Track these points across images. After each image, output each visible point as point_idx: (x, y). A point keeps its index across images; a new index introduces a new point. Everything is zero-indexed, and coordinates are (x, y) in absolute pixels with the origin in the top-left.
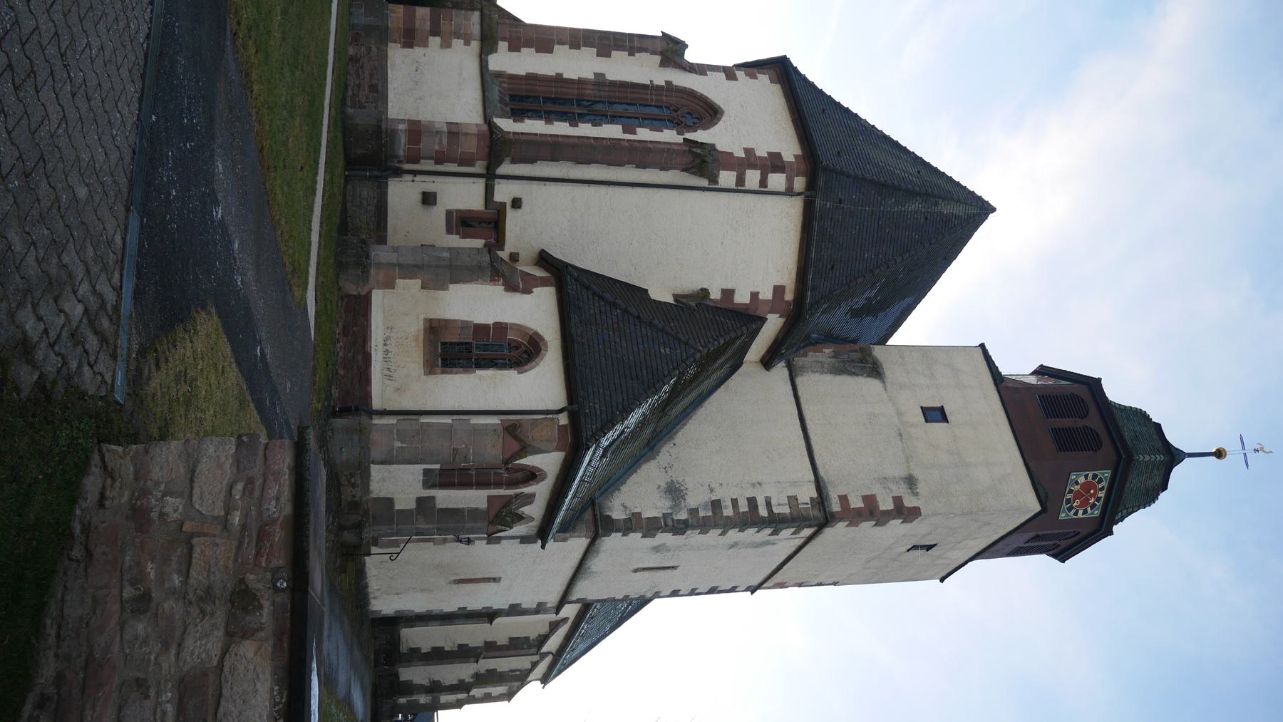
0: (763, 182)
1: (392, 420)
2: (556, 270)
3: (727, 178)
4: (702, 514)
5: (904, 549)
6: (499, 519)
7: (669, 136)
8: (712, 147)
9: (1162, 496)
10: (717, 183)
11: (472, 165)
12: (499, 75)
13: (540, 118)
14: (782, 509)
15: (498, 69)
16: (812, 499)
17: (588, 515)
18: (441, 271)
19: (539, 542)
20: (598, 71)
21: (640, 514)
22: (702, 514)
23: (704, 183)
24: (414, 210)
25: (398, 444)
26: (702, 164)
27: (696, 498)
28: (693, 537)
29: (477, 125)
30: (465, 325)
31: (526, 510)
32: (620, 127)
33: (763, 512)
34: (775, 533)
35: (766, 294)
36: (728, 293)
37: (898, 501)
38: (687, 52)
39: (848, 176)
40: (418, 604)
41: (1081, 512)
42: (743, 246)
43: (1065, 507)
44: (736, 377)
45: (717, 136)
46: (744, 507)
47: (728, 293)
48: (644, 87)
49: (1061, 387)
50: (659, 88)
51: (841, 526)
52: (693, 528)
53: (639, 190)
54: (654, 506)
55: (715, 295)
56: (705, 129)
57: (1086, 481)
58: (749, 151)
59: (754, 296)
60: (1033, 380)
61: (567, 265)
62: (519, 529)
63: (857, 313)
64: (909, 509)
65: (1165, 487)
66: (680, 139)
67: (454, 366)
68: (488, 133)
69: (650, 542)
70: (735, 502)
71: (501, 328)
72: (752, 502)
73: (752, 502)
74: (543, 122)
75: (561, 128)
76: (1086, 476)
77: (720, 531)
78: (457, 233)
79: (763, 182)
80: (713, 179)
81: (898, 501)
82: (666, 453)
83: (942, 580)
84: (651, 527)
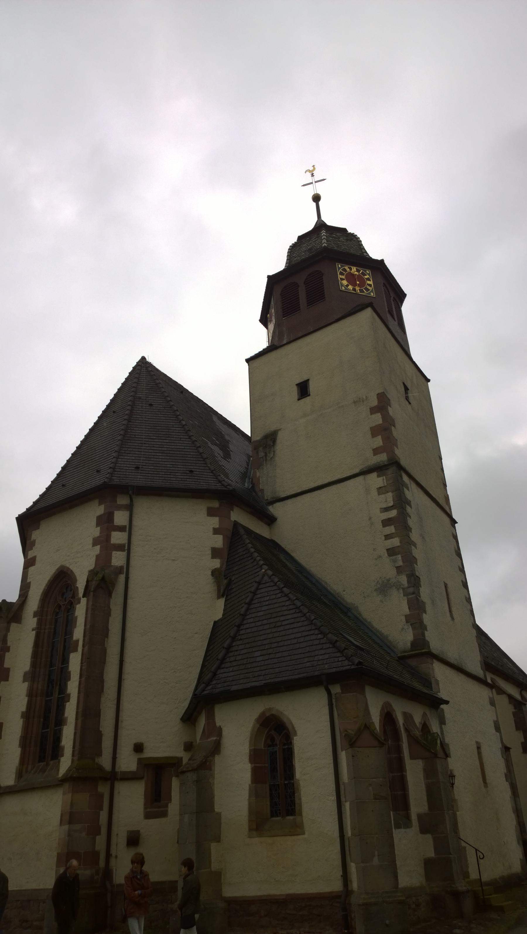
0: (121, 529)
1: (353, 868)
2: (203, 703)
3: (118, 559)
4: (400, 563)
5: (409, 407)
6: (432, 749)
7: (81, 611)
8: (93, 573)
9: (350, 231)
10: (122, 568)
11: (101, 796)
12: (20, 774)
13: (60, 731)
14: (389, 499)
15: (14, 776)
16: (378, 476)
17: (413, 662)
18: (204, 819)
19: (442, 706)
20: (21, 679)
21: (406, 616)
22: (400, 563)
23: (122, 578)
24: (145, 835)
25: (376, 861)
26: (105, 582)
27: (388, 569)
28: (421, 569)
29: (64, 794)
30: (254, 793)
31: (418, 720)
33: (393, 513)
34: (409, 503)
35: (215, 522)
36: (215, 553)
37: (373, 410)
38: (9, 600)
40: (509, 821)
41: (368, 282)
42: (175, 550)
44: (283, 545)
45: (82, 570)
46: (391, 529)
47: (215, 553)
48: (37, 636)
49: (276, 312)
50: (39, 623)
51: (398, 452)
53: (128, 634)
54: (400, 605)
55: (216, 563)
56: (76, 580)
57: (343, 278)
58: (95, 542)
59: (216, 531)
60: (271, 326)
61: (195, 695)
62: (435, 728)
63: (227, 455)
64: (379, 401)
65: (344, 230)
66: (84, 601)
67: (293, 803)
69: (429, 607)
70: (388, 537)
71: (255, 756)
72: (386, 523)
73: (386, 523)
75: (71, 710)
76: (342, 279)
77: (413, 547)
78: (166, 806)
79: (121, 529)
80: (119, 570)
81: (373, 410)
82: (351, 597)
83: (429, 380)
84: (417, 607)
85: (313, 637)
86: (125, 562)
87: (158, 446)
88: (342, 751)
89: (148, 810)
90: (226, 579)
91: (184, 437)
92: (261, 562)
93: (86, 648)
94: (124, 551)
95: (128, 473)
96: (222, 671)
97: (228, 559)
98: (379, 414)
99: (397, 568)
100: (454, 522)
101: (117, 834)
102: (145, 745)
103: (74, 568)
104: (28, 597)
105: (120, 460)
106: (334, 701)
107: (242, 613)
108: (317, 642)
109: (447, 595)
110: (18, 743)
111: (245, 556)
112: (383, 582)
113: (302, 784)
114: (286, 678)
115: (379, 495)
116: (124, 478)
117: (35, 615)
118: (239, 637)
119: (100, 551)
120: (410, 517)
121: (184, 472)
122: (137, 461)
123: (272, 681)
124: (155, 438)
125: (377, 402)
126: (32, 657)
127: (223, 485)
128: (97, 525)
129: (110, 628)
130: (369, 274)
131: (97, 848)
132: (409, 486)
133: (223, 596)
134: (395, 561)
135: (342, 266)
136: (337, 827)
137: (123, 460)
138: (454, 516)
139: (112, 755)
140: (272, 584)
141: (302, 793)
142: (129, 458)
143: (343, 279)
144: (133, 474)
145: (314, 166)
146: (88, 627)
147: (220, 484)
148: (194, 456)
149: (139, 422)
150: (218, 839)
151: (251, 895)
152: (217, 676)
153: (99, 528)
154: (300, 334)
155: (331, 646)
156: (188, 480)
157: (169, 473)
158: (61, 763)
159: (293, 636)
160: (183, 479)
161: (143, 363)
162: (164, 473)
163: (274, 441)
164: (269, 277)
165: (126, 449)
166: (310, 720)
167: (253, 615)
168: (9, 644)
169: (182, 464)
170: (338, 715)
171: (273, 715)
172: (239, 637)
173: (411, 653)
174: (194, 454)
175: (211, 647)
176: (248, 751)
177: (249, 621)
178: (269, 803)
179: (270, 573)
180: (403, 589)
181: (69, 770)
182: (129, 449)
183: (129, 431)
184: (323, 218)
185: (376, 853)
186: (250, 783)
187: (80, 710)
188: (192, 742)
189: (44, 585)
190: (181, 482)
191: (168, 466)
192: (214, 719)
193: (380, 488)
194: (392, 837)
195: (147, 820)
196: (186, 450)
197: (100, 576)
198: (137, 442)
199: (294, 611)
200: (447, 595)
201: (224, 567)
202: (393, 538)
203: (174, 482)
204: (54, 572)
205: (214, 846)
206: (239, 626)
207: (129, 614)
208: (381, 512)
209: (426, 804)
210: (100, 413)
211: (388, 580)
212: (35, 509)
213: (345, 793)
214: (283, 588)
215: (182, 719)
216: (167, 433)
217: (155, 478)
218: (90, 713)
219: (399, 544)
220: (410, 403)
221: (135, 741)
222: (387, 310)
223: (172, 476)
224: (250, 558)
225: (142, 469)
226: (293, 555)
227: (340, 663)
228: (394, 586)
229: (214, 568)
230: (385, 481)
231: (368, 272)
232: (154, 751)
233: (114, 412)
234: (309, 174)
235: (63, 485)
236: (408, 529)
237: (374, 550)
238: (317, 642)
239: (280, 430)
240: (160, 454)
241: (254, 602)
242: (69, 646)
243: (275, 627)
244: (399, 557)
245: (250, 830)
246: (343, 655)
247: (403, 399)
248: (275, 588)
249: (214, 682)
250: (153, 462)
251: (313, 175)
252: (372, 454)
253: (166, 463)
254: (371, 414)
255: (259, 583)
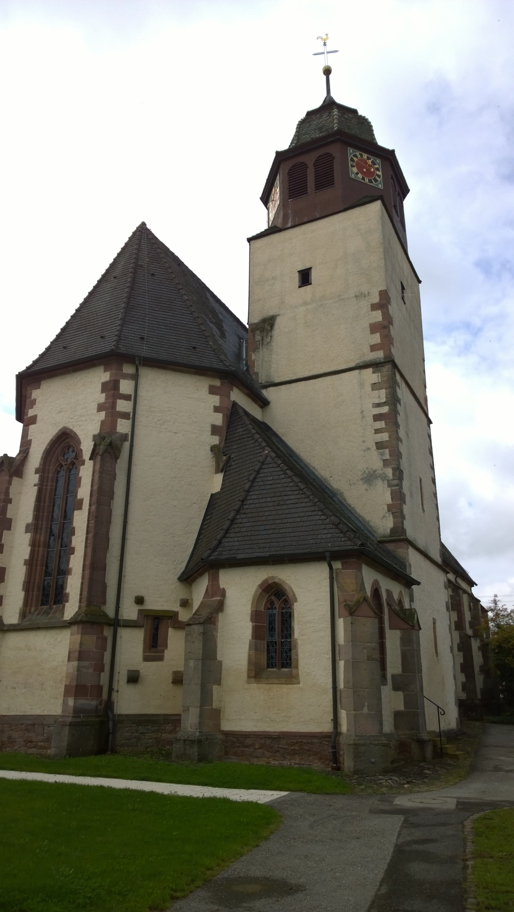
0: (127, 398)
1: (343, 714)
3: (123, 427)
4: (387, 457)
5: (404, 306)
7: (86, 473)
8: (98, 439)
9: (361, 112)
10: (126, 435)
11: (105, 639)
12: (23, 615)
14: (382, 395)
15: (17, 616)
16: (374, 372)
17: (391, 547)
19: (414, 587)
20: (24, 529)
22: (387, 457)
23: (127, 444)
25: (365, 710)
26: (111, 448)
27: (375, 461)
29: (72, 634)
30: (254, 647)
32: (76, 513)
33: (385, 409)
35: (215, 400)
36: (215, 430)
37: (374, 307)
38: (9, 455)
39: (121, 331)
41: (378, 173)
42: (177, 419)
43: (374, 184)
45: (87, 431)
46: (381, 424)
47: (215, 430)
48: (40, 492)
50: (41, 479)
52: (399, 464)
53: (131, 498)
54: (383, 495)
55: (216, 440)
56: (79, 443)
57: (355, 166)
58: (100, 408)
59: (216, 409)
63: (223, 335)
64: (381, 299)
68: (81, 626)
70: (377, 431)
71: (256, 616)
72: (377, 418)
73: (377, 418)
74: (69, 577)
75: (77, 563)
76: (352, 166)
77: (400, 443)
78: (163, 652)
79: (127, 398)
80: (124, 437)
81: (374, 307)
82: (337, 483)
83: (420, 282)
85: (318, 518)
86: (130, 430)
87: (161, 318)
88: (339, 618)
89: (147, 654)
90: (225, 455)
91: (187, 312)
92: (264, 444)
93: (94, 507)
94: (129, 419)
95: (133, 343)
96: (227, 540)
97: (226, 437)
98: (380, 311)
99: (384, 461)
100: (430, 422)
101: (119, 672)
102: (145, 598)
103: (77, 430)
104: (30, 454)
105: (125, 328)
106: (334, 575)
107: (246, 489)
108: (321, 522)
109: (421, 489)
110: (22, 587)
111: (245, 436)
112: (369, 472)
113: (299, 642)
114: (291, 552)
115: (372, 390)
116: (131, 348)
117: (37, 471)
118: (243, 511)
119: (106, 417)
120: (399, 414)
121: (187, 347)
122: (141, 331)
123: (277, 553)
124: (158, 309)
125: (379, 299)
126: (34, 511)
127: (224, 365)
128: (103, 391)
129: (115, 491)
130: (379, 164)
131: (101, 683)
132: (400, 385)
133: (222, 471)
134: (382, 454)
135: (353, 152)
136: (331, 680)
137: (128, 329)
138: (430, 416)
139: (115, 605)
140: (275, 465)
141: (299, 650)
142: (133, 327)
143: (354, 166)
144: (138, 344)
145: (327, 35)
146: (95, 488)
147: (222, 364)
148: (196, 333)
149: (142, 291)
150: (219, 682)
151: (247, 730)
152: (222, 544)
153: (104, 395)
154: (306, 220)
155: (334, 527)
156: (191, 356)
157: (173, 348)
158: (66, 608)
159: (297, 515)
160: (187, 355)
161: (143, 229)
162: (168, 347)
163: (272, 326)
164: (278, 154)
165: (130, 318)
166: (310, 589)
167: (257, 493)
168: (11, 496)
169: (185, 339)
170: (338, 587)
171: (275, 583)
172: (243, 511)
173: (390, 538)
174: (196, 330)
175: (208, 517)
176: (250, 612)
177: (253, 497)
178: (266, 657)
179: (273, 455)
180: (388, 481)
181: (77, 614)
182: (133, 318)
183: (132, 299)
184: (333, 94)
185: (366, 704)
186: (250, 638)
187: (88, 562)
188: (188, 600)
189: (46, 444)
190: (185, 357)
191: (172, 340)
192: (218, 581)
193: (375, 384)
194: (380, 692)
195: (145, 663)
196: (188, 326)
197: (108, 441)
198: (140, 312)
199: (297, 492)
200: (421, 489)
201: (223, 444)
202: (382, 432)
203: (178, 356)
204: (56, 432)
205: (215, 687)
206: (243, 501)
207: (133, 479)
208: (373, 407)
209: (400, 666)
210: (100, 277)
211: (375, 471)
212: (36, 368)
213: (339, 653)
214: (286, 470)
215: (178, 579)
216: (170, 306)
217: (160, 351)
218: (95, 566)
219: (387, 439)
220: (405, 303)
221: (137, 594)
222: (393, 204)
223: (176, 351)
224: (251, 439)
225: (147, 340)
226: (284, 438)
227: (343, 543)
228: (380, 477)
229: (213, 444)
230: (380, 377)
231: (378, 161)
232: (156, 603)
233: (115, 278)
234: (322, 43)
235: (64, 348)
236: (397, 426)
237: (364, 441)
238: (321, 522)
239: (279, 315)
240: (164, 327)
241: (257, 480)
242: (72, 504)
243: (278, 505)
244: (387, 451)
245: (249, 677)
246: (346, 536)
247: (400, 299)
248: (278, 469)
249: (220, 549)
250: (157, 334)
251: (325, 44)
252: (370, 350)
253: (169, 337)
254: (372, 311)
255: (263, 463)
